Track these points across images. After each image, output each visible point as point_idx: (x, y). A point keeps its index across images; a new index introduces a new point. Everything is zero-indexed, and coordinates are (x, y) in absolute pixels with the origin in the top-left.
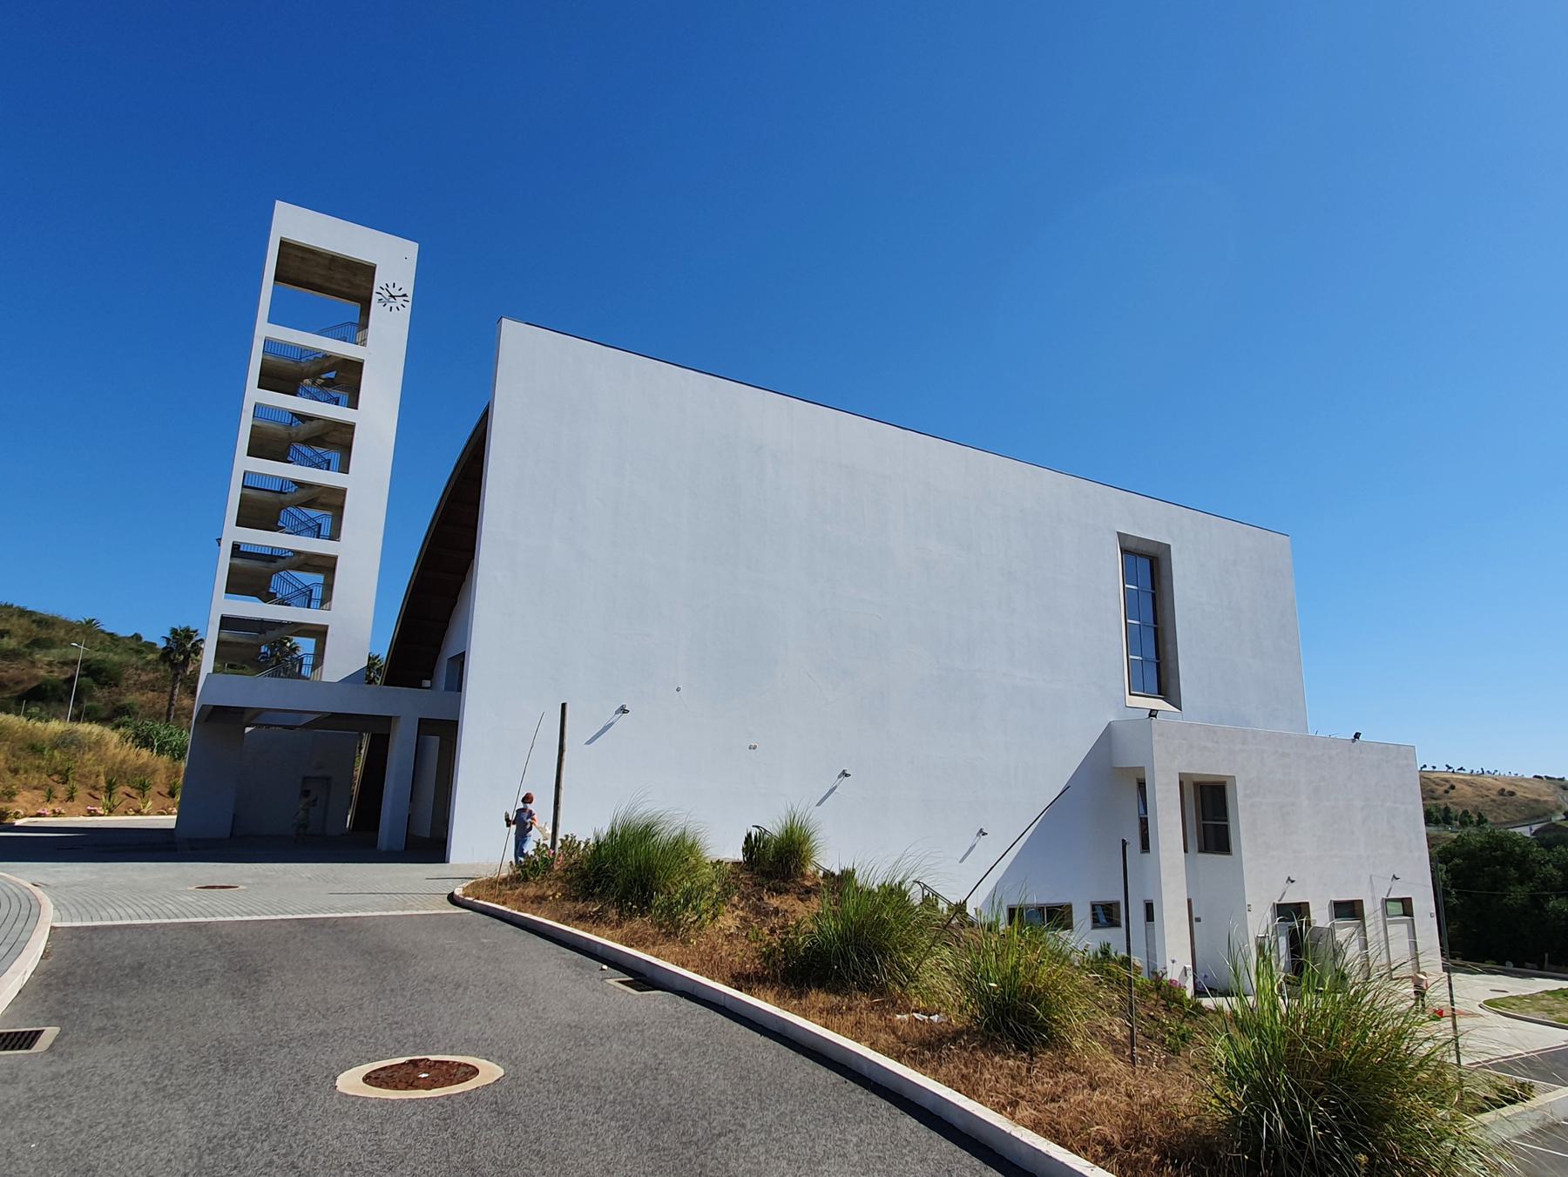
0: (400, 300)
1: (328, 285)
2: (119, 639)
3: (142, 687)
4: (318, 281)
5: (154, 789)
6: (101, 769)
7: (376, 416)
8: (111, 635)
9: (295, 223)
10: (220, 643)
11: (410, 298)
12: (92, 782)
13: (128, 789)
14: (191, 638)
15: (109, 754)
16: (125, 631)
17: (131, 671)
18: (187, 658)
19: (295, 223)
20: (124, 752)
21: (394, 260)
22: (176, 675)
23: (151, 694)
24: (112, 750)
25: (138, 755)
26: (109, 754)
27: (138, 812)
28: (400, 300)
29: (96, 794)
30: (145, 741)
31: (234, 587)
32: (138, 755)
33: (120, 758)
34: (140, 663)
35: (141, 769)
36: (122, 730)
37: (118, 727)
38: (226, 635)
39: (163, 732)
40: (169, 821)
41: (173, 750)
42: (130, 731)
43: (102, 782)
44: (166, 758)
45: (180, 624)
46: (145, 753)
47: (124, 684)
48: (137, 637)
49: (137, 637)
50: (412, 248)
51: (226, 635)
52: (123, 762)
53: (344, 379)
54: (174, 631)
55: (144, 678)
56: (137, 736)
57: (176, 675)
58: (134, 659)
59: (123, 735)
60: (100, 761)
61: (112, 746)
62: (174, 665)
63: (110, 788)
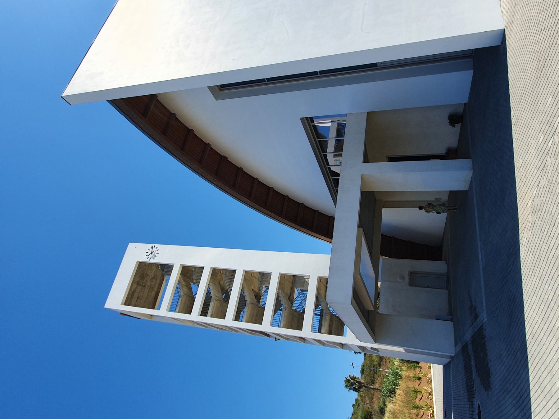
0: (154, 249)
1: (155, 289)
2: (354, 412)
3: (371, 402)
4: (153, 294)
5: (417, 386)
6: (407, 412)
7: (208, 258)
8: (352, 415)
9: (116, 300)
10: (330, 333)
11: (154, 245)
12: (414, 416)
13: (418, 399)
14: (349, 380)
15: (399, 408)
16: (352, 410)
17: (365, 406)
18: (357, 382)
19: (116, 300)
20: (398, 402)
21: (136, 253)
22: (365, 387)
23: (374, 399)
24: (397, 407)
25: (399, 395)
26: (399, 408)
27: (430, 394)
28: (154, 249)
29: (421, 414)
30: (393, 391)
31: (299, 327)
32: (399, 395)
33: (400, 403)
34: (363, 403)
35: (407, 393)
36: (386, 403)
37: (385, 405)
38: (324, 329)
39: (387, 383)
40: (436, 373)
41: (396, 379)
42: (388, 399)
43: (415, 411)
44: (400, 382)
45: (343, 384)
46: (398, 392)
47: (370, 410)
48: (353, 406)
49: (353, 406)
50: (131, 246)
51: (325, 328)
52: (403, 402)
53: (190, 274)
54: (346, 386)
55: (368, 402)
56: (390, 396)
57: (365, 387)
58: (361, 406)
59: (389, 402)
60: (403, 413)
61: (395, 407)
62: (360, 387)
63: (418, 407)
